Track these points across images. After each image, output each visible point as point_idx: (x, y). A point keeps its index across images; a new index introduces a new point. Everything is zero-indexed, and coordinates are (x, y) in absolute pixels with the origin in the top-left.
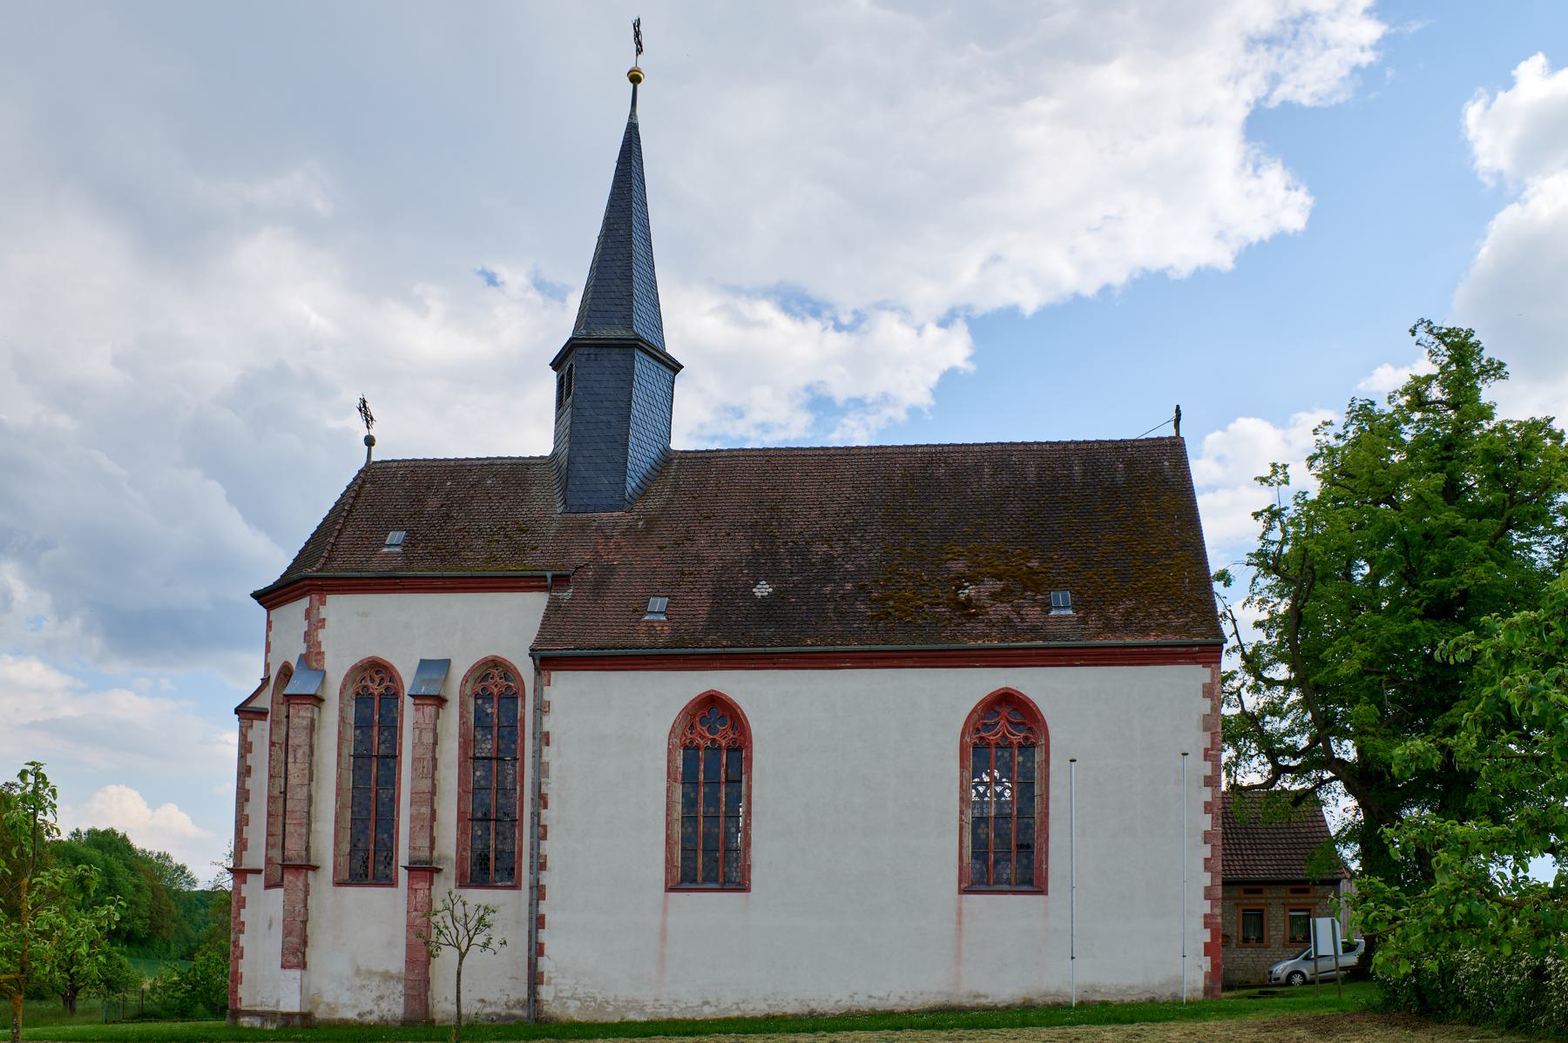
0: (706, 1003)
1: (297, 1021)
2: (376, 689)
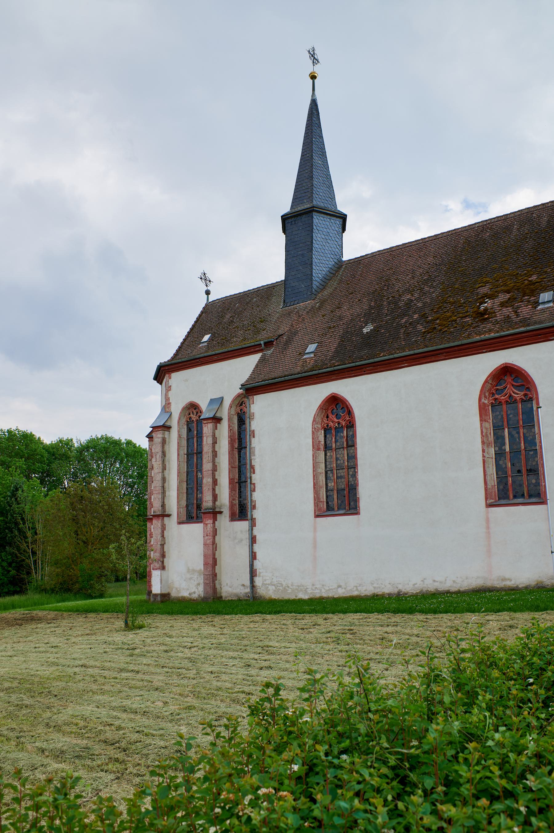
0: (339, 586)
1: (159, 598)
2: (194, 418)
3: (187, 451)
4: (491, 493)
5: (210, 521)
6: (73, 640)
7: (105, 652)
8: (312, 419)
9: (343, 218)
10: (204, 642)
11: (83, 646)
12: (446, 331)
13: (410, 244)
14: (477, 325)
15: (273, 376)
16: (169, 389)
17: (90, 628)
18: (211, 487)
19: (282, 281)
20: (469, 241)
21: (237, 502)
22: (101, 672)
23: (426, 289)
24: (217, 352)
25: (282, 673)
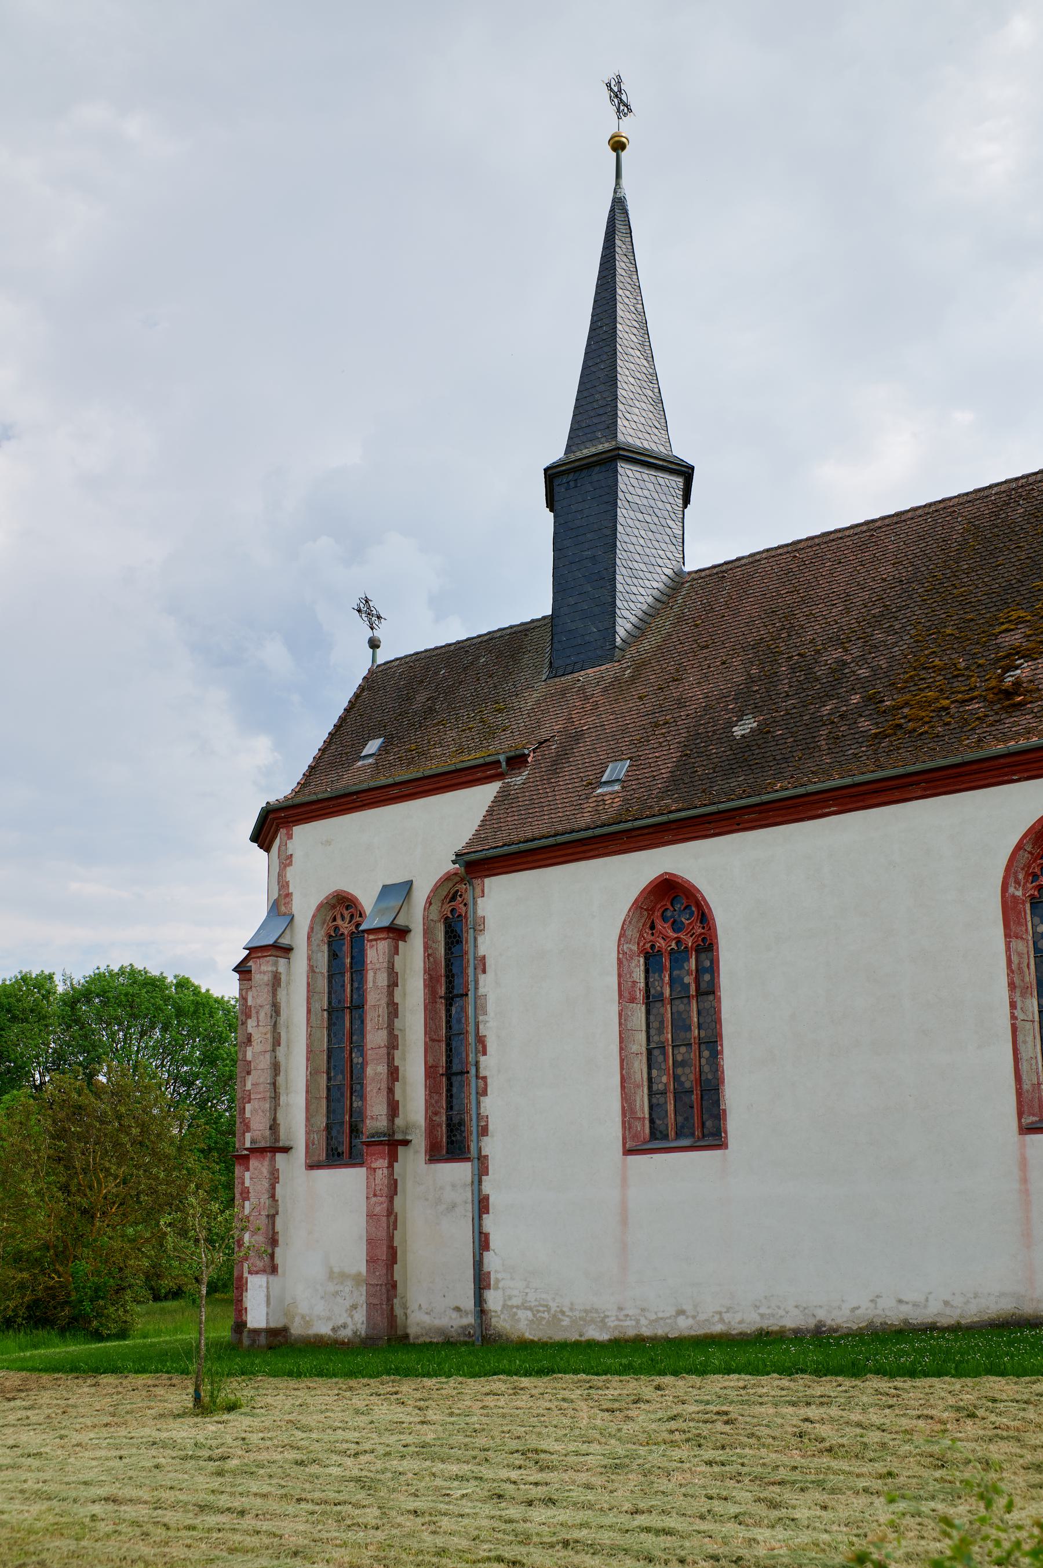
0: (681, 1312)
1: (262, 1340)
2: (346, 928)
3: (330, 1003)
4: (1032, 1101)
5: (382, 1163)
6: (76, 1438)
7: (157, 1467)
8: (618, 931)
9: (686, 473)
10: (384, 1440)
11: (99, 1453)
12: (926, 732)
13: (840, 535)
14: (997, 718)
15: (529, 835)
16: (286, 861)
17: (112, 1409)
18: (384, 1086)
19: (544, 618)
20: (977, 527)
21: (444, 1118)
22: (155, 1514)
23: (879, 636)
24: (398, 779)
25: (581, 1513)
